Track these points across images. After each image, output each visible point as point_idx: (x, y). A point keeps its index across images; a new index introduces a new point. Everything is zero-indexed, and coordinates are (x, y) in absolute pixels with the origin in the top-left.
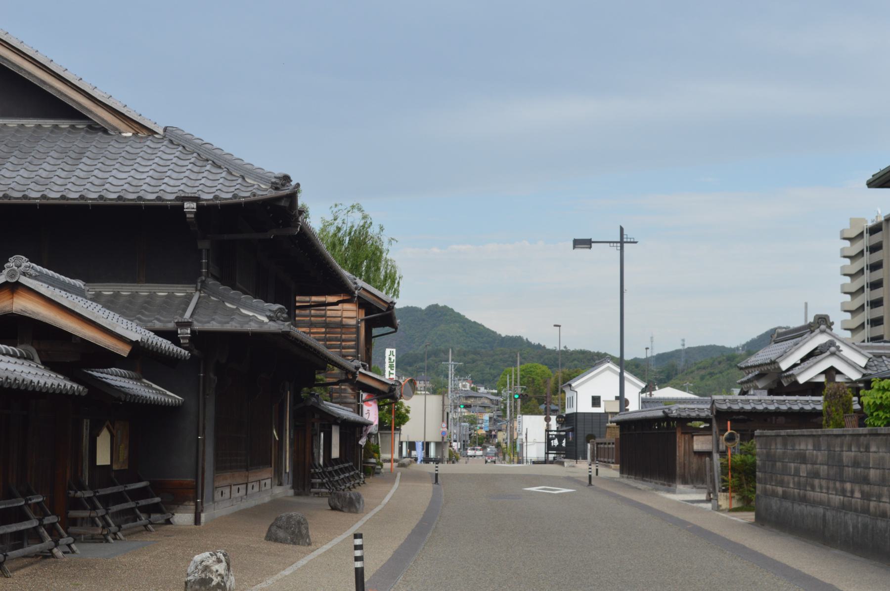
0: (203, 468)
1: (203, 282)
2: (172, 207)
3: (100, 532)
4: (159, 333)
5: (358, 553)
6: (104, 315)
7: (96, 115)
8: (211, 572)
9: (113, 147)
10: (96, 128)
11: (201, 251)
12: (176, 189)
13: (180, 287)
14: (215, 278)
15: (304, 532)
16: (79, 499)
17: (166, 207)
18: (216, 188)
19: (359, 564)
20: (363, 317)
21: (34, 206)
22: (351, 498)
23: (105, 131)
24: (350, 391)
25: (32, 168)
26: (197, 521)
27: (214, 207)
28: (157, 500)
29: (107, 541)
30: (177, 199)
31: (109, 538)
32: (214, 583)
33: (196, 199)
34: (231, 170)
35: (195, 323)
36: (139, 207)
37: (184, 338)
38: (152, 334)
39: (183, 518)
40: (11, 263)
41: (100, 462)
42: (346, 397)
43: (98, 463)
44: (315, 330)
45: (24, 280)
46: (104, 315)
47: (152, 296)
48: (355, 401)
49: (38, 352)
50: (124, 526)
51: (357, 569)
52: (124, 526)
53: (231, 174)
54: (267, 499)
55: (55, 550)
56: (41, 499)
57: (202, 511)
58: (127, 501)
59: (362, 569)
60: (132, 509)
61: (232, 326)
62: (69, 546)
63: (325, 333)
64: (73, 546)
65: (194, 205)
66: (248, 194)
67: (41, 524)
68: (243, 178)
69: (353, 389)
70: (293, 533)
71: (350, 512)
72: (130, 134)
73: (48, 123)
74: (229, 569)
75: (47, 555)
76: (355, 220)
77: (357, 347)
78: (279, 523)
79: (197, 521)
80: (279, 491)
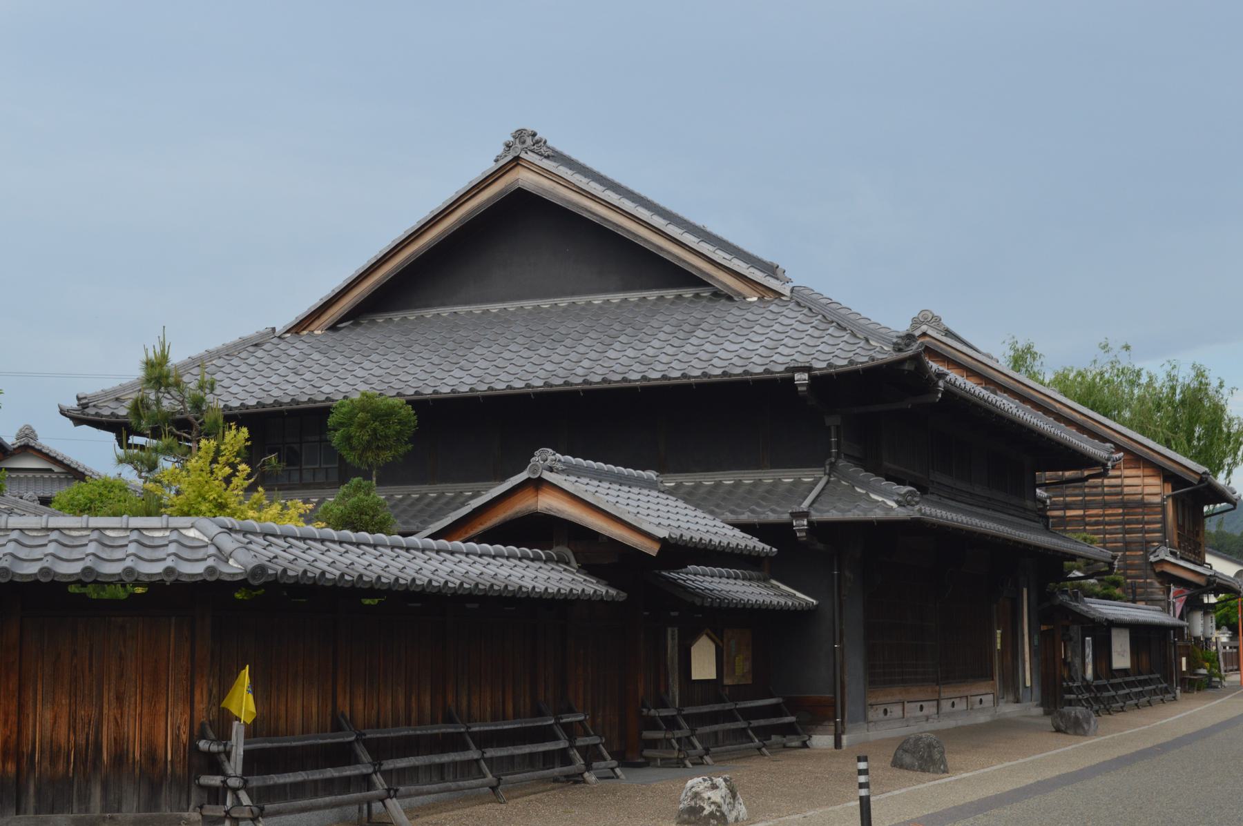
0: (842, 683)
1: (832, 465)
2: (783, 379)
3: (676, 755)
4: (745, 528)
5: (862, 779)
6: (646, 508)
7: (718, 281)
8: (702, 799)
9: (733, 313)
10: (718, 295)
11: (829, 428)
12: (788, 359)
13: (807, 471)
14: (849, 457)
15: (937, 756)
16: (653, 717)
17: (775, 380)
18: (834, 353)
19: (863, 792)
20: (1170, 492)
21: (634, 389)
22: (1077, 718)
23: (730, 298)
24: (1157, 585)
25: (640, 346)
26: (838, 744)
27: (829, 376)
28: (791, 719)
29: (685, 766)
30: (787, 370)
31: (687, 762)
32: (706, 812)
33: (808, 369)
34: (855, 331)
35: (813, 512)
36: (746, 382)
37: (800, 531)
38: (737, 532)
39: (822, 741)
40: (537, 459)
41: (697, 675)
42: (1152, 593)
43: (695, 676)
44: (1110, 512)
45: (547, 476)
46: (646, 508)
47: (777, 483)
48: (1164, 597)
49: (575, 554)
50: (712, 750)
51: (861, 798)
52: (712, 750)
53: (855, 336)
54: (982, 718)
55: (586, 775)
56: (582, 718)
57: (843, 733)
58: (737, 720)
59: (868, 798)
60: (744, 729)
61: (854, 514)
62: (613, 769)
63: (1123, 514)
64: (618, 771)
65: (806, 376)
66: (866, 359)
67: (572, 746)
68: (867, 340)
69: (1161, 583)
70: (922, 757)
71: (1076, 734)
72: (755, 299)
73: (670, 294)
74: (734, 797)
75: (576, 779)
76: (1185, 376)
77: (1164, 530)
78: (906, 746)
79: (838, 744)
80: (1009, 709)
